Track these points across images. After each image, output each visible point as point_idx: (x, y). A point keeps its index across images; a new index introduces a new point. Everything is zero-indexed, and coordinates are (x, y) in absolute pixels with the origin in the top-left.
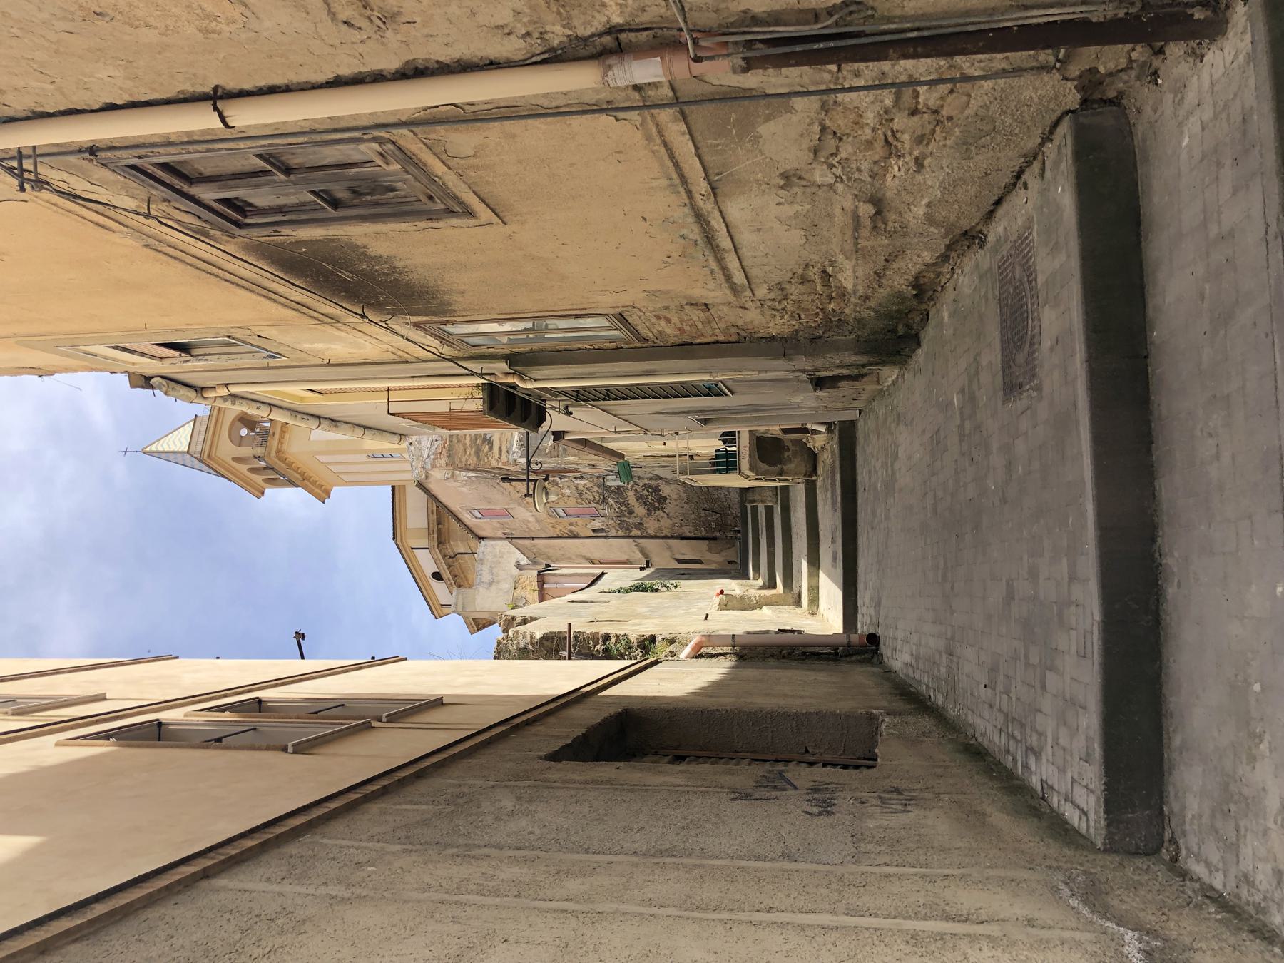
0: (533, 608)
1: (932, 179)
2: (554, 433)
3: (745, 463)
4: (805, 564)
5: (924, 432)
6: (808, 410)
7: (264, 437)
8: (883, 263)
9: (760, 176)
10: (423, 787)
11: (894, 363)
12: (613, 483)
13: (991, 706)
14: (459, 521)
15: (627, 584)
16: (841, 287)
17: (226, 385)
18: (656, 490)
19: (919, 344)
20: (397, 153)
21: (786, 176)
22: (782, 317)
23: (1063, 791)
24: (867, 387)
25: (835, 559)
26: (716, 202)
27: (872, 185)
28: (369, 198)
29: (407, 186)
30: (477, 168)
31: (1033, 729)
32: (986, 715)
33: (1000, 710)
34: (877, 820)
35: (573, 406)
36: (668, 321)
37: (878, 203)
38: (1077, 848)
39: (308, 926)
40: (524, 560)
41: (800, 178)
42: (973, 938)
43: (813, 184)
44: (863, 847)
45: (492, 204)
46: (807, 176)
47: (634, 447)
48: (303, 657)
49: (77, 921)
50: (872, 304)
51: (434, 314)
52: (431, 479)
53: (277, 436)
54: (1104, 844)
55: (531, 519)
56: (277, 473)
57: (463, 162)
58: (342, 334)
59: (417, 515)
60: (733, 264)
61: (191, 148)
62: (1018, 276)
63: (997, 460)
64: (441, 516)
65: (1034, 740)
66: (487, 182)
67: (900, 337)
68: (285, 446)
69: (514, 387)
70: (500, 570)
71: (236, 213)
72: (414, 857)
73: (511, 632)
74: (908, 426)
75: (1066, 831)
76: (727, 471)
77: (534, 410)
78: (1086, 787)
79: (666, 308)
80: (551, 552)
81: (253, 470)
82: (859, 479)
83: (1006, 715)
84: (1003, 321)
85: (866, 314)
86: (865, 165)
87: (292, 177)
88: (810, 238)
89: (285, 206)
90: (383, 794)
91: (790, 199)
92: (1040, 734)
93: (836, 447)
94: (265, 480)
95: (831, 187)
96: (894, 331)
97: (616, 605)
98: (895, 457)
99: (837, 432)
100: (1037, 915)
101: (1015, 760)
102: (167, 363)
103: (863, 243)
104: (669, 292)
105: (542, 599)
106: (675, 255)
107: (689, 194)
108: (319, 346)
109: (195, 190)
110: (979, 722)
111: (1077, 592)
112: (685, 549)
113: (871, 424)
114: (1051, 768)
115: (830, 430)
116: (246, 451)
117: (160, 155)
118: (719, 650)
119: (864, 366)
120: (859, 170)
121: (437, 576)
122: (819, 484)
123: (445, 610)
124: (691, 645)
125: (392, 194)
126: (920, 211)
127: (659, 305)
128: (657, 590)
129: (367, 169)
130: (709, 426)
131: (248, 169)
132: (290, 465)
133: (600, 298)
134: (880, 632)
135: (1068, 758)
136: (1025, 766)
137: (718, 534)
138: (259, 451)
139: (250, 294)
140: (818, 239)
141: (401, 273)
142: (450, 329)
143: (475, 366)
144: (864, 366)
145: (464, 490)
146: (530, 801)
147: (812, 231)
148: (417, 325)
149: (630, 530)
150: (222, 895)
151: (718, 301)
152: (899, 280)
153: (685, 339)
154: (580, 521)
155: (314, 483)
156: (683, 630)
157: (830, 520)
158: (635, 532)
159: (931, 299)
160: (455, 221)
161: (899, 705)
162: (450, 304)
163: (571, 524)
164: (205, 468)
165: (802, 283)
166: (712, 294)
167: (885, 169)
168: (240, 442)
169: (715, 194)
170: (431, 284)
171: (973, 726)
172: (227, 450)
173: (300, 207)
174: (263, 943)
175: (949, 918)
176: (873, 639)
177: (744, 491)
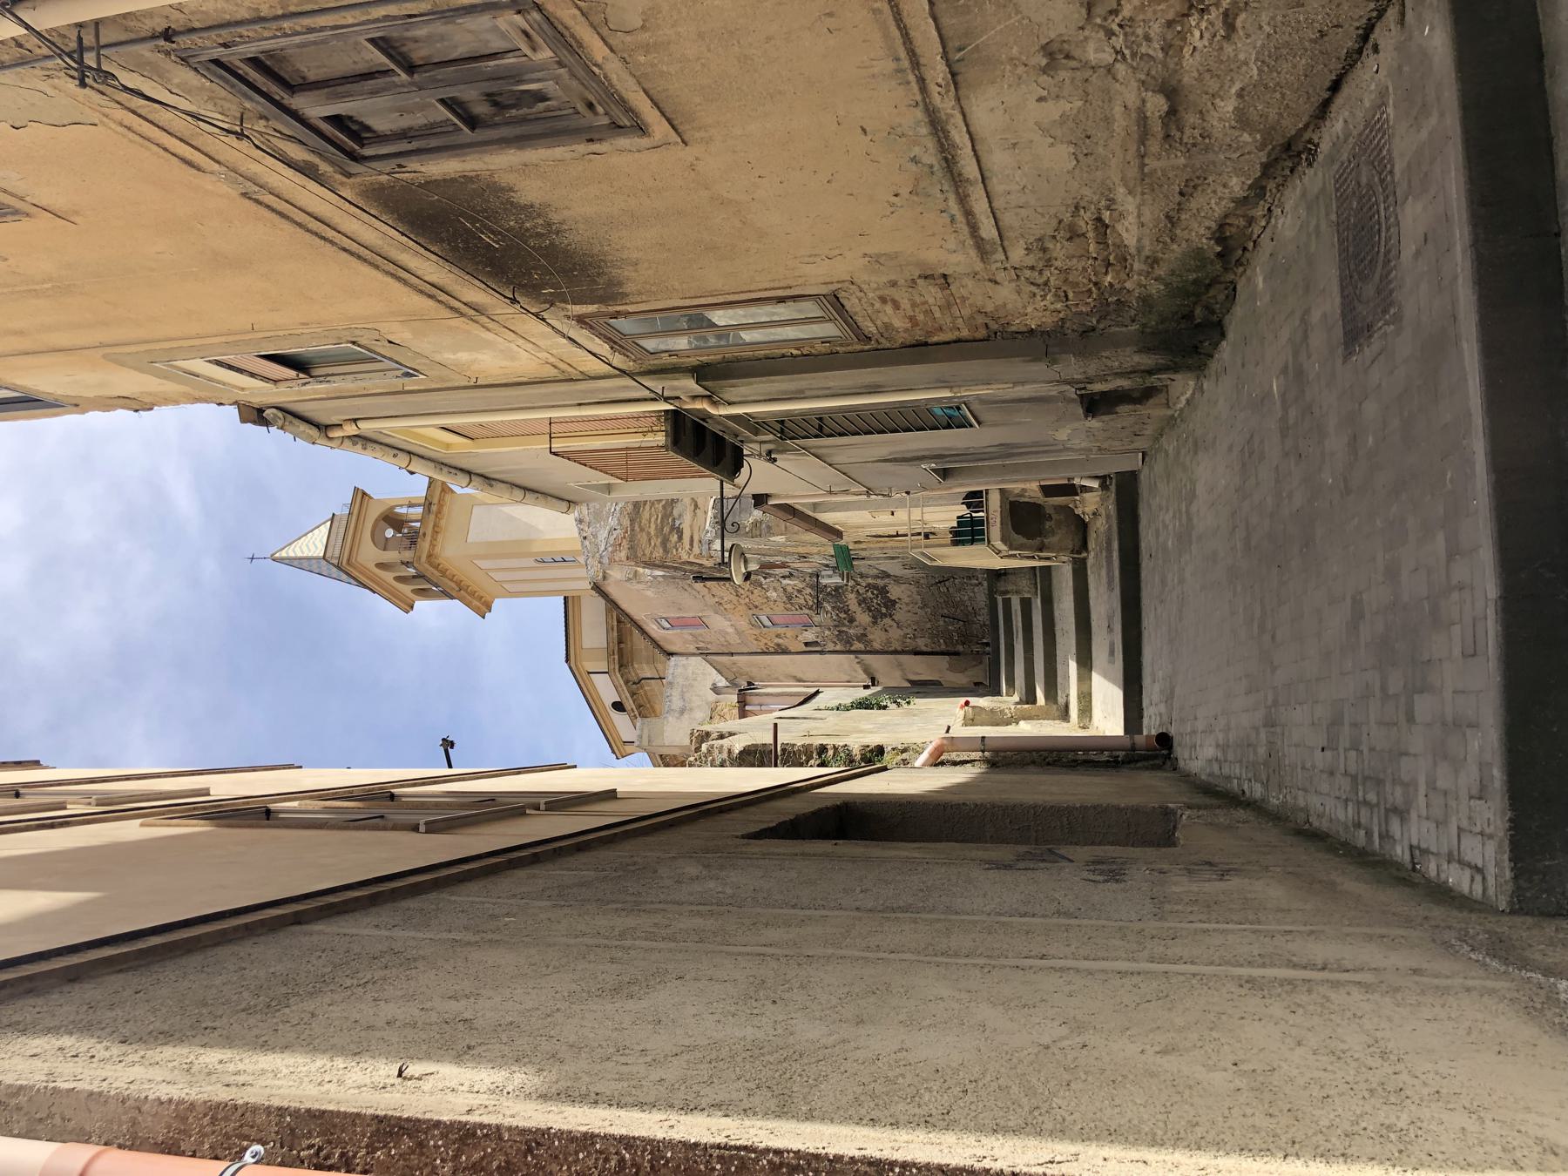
0: (733, 724)
1: (1245, 48)
2: (754, 496)
3: (995, 531)
4: (1073, 666)
5: (1230, 449)
6: (1078, 447)
7: (413, 539)
8: (1178, 198)
9: (1015, 50)
10: (584, 858)
11: (1189, 368)
12: (831, 580)
13: (1332, 774)
14: (643, 632)
15: (848, 701)
16: (1121, 246)
17: (355, 420)
18: (883, 591)
19: (1223, 335)
20: (545, 26)
21: (1047, 50)
22: (1044, 297)
23: (1445, 850)
24: (1153, 411)
25: (1112, 653)
26: (958, 99)
27: (1165, 65)
28: (514, 112)
29: (556, 87)
30: (647, 48)
31: (1396, 781)
32: (1325, 787)
33: (1346, 773)
34: (1181, 886)
35: (779, 452)
36: (896, 305)
37: (1171, 92)
38: (1471, 911)
39: (420, 964)
40: (722, 682)
41: (1068, 57)
42: (1336, 985)
43: (1086, 65)
44: (1167, 907)
45: (668, 110)
46: (1076, 53)
47: (859, 520)
48: (450, 766)
49: (124, 949)
50: (1161, 271)
51: (602, 300)
52: (610, 581)
53: (428, 538)
54: (1510, 903)
55: (731, 630)
56: (429, 581)
57: (628, 38)
58: (490, 336)
59: (595, 633)
60: (980, 206)
61: (286, 25)
62: (1364, 180)
63: (1336, 443)
64: (622, 624)
65: (1397, 795)
66: (662, 73)
67: (1199, 325)
68: (437, 550)
69: (706, 416)
70: (693, 686)
71: (349, 139)
72: (566, 910)
73: (704, 747)
74: (1210, 459)
75: (1453, 898)
76: (972, 542)
77: (728, 452)
78: (1482, 834)
79: (894, 284)
80: (754, 672)
81: (399, 579)
82: (1143, 545)
83: (1354, 778)
84: (1343, 250)
85: (1155, 288)
86: (1156, 29)
87: (416, 76)
88: (1081, 157)
89: (411, 129)
90: (533, 863)
91: (1054, 90)
92: (1405, 785)
93: (1112, 508)
94: (414, 591)
95: (1109, 69)
96: (1188, 317)
97: (834, 721)
98: (1192, 496)
99: (1113, 488)
100: (1425, 966)
101: (1369, 834)
102: (282, 388)
103: (1152, 163)
104: (895, 256)
105: (743, 714)
106: (904, 192)
107: (923, 89)
108: (464, 356)
109: (298, 102)
110: (1314, 801)
111: (1461, 572)
112: (922, 668)
113: (1159, 467)
114: (1426, 825)
115: (1104, 486)
116: (391, 556)
117: (251, 40)
118: (964, 756)
119: (1150, 372)
120: (1147, 38)
121: (618, 706)
122: (1090, 562)
123: (628, 748)
124: (930, 748)
125: (541, 106)
126: (1228, 106)
127: (884, 279)
128: (885, 707)
129: (510, 60)
130: (949, 482)
131: (362, 68)
132: (443, 573)
133: (808, 269)
134: (1173, 731)
135: (1453, 804)
136: (1386, 836)
137: (960, 648)
138: (408, 555)
139: (374, 272)
140: (1091, 159)
141: (557, 233)
142: (619, 323)
143: (656, 384)
144: (1150, 372)
145: (649, 593)
146: (722, 868)
147: (1083, 147)
148: (581, 320)
149: (849, 643)
150: (315, 938)
151: (960, 269)
152: (1197, 234)
153: (919, 335)
154: (790, 633)
155: (472, 594)
156: (919, 741)
157: (1105, 604)
158: (858, 646)
159: (1239, 263)
160: (623, 142)
161: (1199, 799)
162: (620, 284)
163: (778, 636)
164: (344, 577)
165: (1070, 239)
166: (954, 258)
167: (1182, 36)
168: (385, 545)
169: (956, 84)
170: (595, 251)
171: (1306, 810)
172: (369, 554)
173: (429, 130)
174: (360, 975)
175: (1295, 966)
176: (1164, 740)
177: (997, 575)
